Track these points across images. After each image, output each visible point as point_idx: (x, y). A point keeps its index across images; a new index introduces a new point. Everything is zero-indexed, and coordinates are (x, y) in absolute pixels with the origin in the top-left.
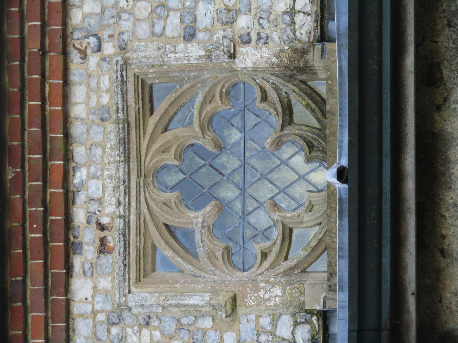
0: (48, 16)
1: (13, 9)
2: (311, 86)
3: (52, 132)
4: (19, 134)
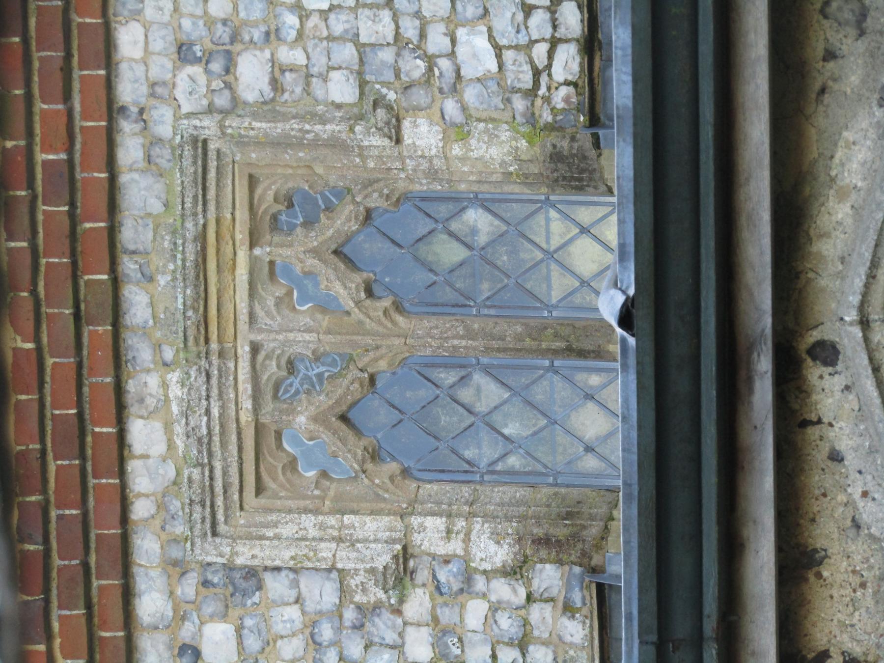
0: (93, 448)
1: (19, 193)
2: (548, 52)
3: (104, 626)
4: (40, 580)
